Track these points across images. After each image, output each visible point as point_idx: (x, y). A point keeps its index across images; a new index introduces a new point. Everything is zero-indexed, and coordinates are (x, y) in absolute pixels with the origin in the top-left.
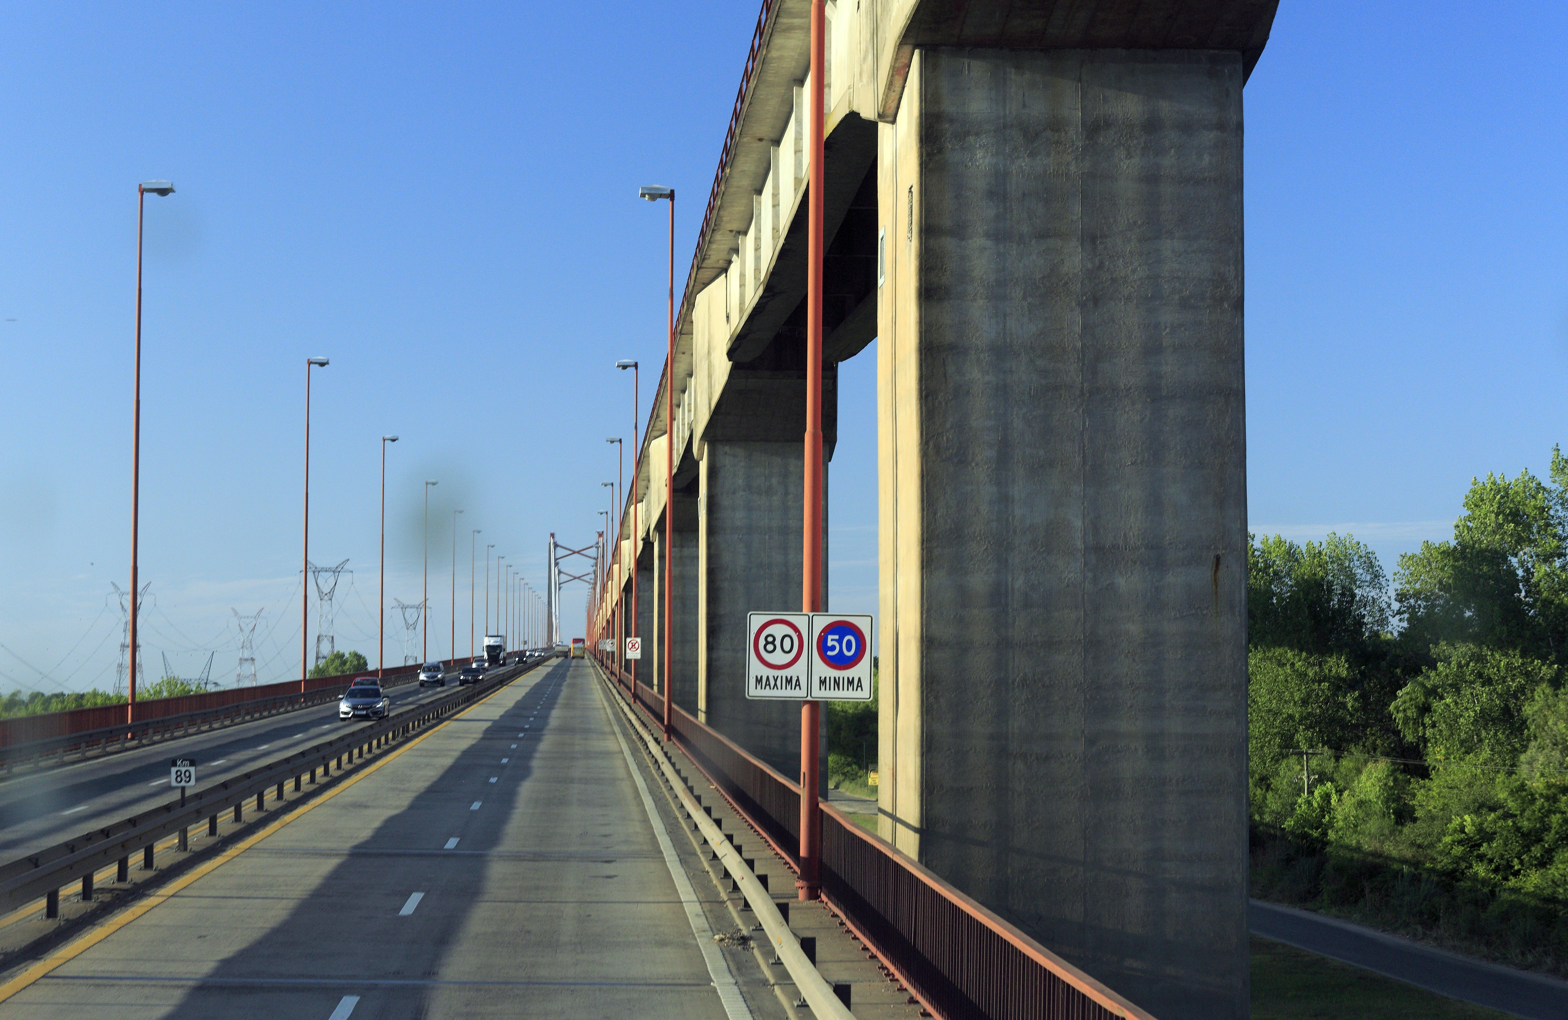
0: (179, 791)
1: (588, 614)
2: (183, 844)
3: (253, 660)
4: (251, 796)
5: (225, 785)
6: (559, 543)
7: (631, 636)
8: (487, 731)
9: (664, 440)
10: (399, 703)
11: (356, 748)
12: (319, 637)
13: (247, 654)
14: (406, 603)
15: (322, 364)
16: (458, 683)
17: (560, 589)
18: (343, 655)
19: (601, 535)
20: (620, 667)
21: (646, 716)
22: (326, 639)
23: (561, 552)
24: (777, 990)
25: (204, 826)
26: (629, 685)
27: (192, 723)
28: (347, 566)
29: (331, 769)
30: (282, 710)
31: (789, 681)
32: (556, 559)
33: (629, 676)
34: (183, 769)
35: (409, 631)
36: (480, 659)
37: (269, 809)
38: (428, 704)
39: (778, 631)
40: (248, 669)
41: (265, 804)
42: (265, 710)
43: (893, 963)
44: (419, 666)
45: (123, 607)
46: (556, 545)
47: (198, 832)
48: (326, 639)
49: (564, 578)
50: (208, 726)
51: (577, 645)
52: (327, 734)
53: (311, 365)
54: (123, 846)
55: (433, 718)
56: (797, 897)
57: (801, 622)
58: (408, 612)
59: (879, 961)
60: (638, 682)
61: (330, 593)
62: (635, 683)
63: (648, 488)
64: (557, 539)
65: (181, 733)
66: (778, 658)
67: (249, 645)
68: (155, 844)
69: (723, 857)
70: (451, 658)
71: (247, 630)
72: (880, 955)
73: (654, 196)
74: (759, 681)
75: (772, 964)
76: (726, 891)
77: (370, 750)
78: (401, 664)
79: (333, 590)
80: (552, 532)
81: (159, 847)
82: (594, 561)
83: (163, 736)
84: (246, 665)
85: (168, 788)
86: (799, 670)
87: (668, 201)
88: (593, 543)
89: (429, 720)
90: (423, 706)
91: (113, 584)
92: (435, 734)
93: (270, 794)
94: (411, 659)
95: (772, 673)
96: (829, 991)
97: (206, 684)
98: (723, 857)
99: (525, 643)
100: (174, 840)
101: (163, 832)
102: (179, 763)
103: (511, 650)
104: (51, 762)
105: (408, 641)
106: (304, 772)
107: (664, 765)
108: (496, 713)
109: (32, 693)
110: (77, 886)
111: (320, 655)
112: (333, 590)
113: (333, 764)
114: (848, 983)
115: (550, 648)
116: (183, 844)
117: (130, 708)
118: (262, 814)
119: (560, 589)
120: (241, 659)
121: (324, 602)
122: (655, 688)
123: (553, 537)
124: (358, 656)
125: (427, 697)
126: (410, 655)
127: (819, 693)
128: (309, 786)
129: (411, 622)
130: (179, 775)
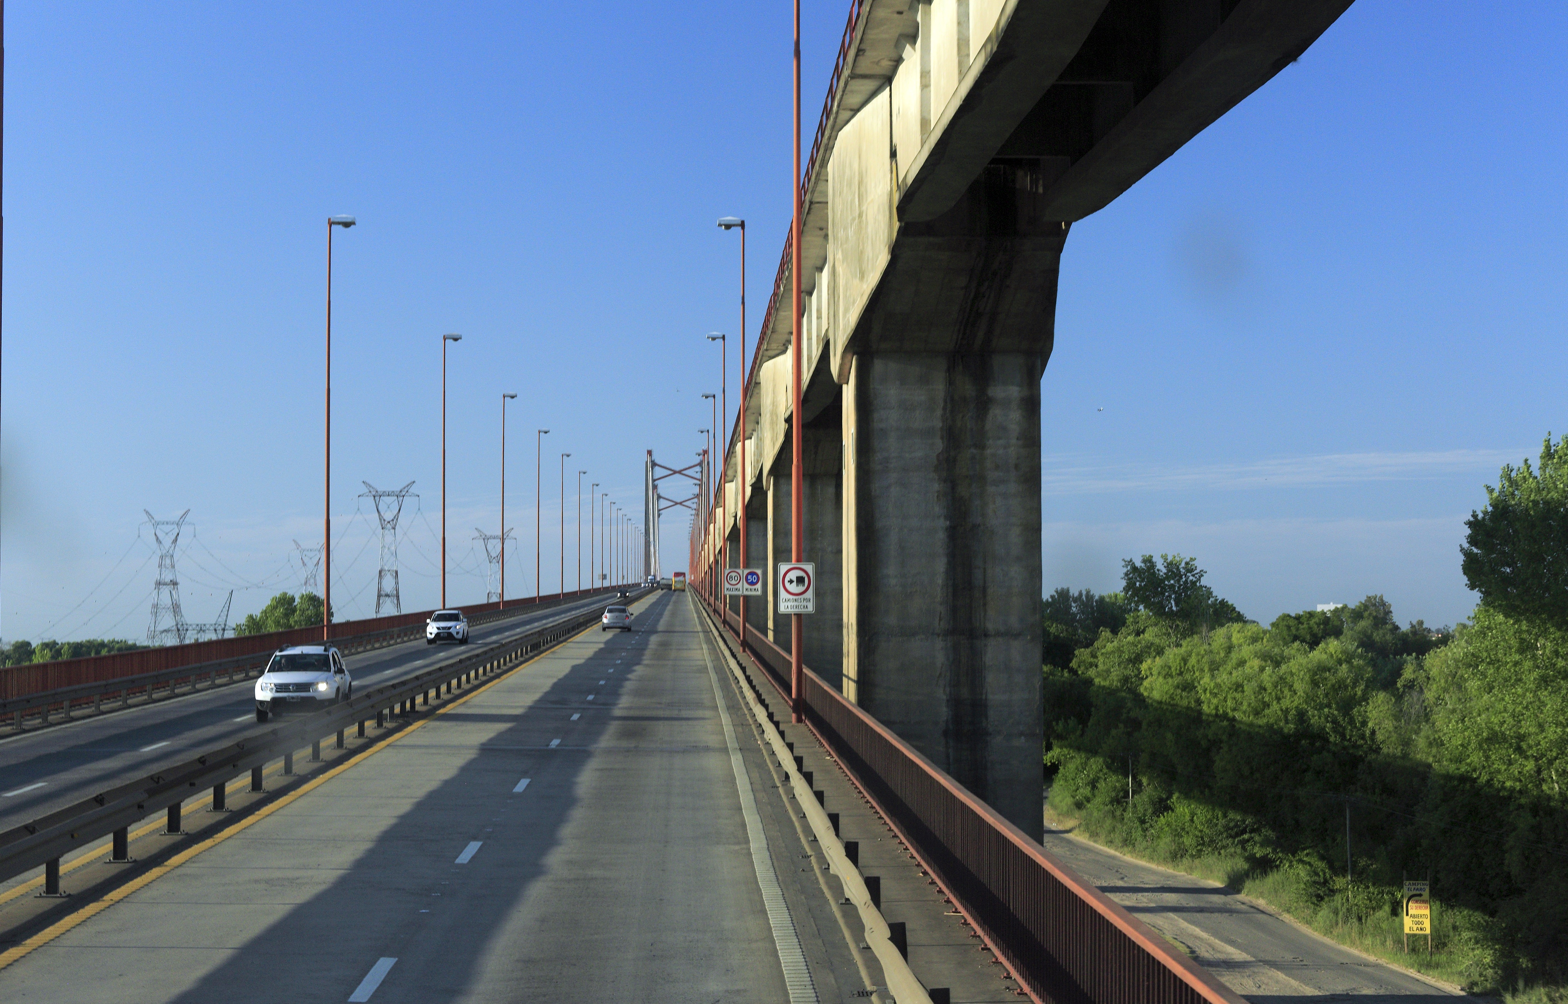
1: (691, 541)
2: (316, 754)
5: (99, 800)
6: (657, 461)
7: (789, 560)
8: (487, 749)
9: (786, 361)
10: (480, 642)
11: (463, 674)
12: (380, 572)
13: (168, 577)
14: (381, 489)
18: (293, 599)
21: (761, 678)
22: (389, 574)
23: (659, 472)
27: (201, 677)
30: (412, 637)
31: (736, 589)
32: (654, 481)
33: (737, 618)
35: (492, 564)
38: (550, 627)
39: (733, 574)
44: (429, 614)
45: (157, 539)
46: (654, 464)
48: (389, 574)
49: (663, 503)
50: (244, 675)
51: (678, 579)
57: (740, 571)
60: (747, 625)
61: (393, 520)
63: (758, 423)
66: (733, 582)
67: (312, 581)
71: (167, 541)
72: (923, 863)
74: (727, 589)
75: (863, 948)
76: (837, 902)
77: (459, 685)
78: (484, 601)
79: (396, 518)
81: (230, 787)
84: (165, 591)
86: (740, 586)
89: (511, 660)
90: (503, 645)
91: (147, 512)
94: (494, 596)
95: (731, 587)
97: (224, 630)
99: (604, 577)
105: (491, 575)
106: (453, 678)
109: (17, 642)
111: (382, 593)
112: (396, 518)
113: (432, 693)
114: (856, 841)
116: (340, 743)
121: (386, 531)
122: (771, 634)
125: (444, 657)
126: (493, 591)
127: (746, 593)
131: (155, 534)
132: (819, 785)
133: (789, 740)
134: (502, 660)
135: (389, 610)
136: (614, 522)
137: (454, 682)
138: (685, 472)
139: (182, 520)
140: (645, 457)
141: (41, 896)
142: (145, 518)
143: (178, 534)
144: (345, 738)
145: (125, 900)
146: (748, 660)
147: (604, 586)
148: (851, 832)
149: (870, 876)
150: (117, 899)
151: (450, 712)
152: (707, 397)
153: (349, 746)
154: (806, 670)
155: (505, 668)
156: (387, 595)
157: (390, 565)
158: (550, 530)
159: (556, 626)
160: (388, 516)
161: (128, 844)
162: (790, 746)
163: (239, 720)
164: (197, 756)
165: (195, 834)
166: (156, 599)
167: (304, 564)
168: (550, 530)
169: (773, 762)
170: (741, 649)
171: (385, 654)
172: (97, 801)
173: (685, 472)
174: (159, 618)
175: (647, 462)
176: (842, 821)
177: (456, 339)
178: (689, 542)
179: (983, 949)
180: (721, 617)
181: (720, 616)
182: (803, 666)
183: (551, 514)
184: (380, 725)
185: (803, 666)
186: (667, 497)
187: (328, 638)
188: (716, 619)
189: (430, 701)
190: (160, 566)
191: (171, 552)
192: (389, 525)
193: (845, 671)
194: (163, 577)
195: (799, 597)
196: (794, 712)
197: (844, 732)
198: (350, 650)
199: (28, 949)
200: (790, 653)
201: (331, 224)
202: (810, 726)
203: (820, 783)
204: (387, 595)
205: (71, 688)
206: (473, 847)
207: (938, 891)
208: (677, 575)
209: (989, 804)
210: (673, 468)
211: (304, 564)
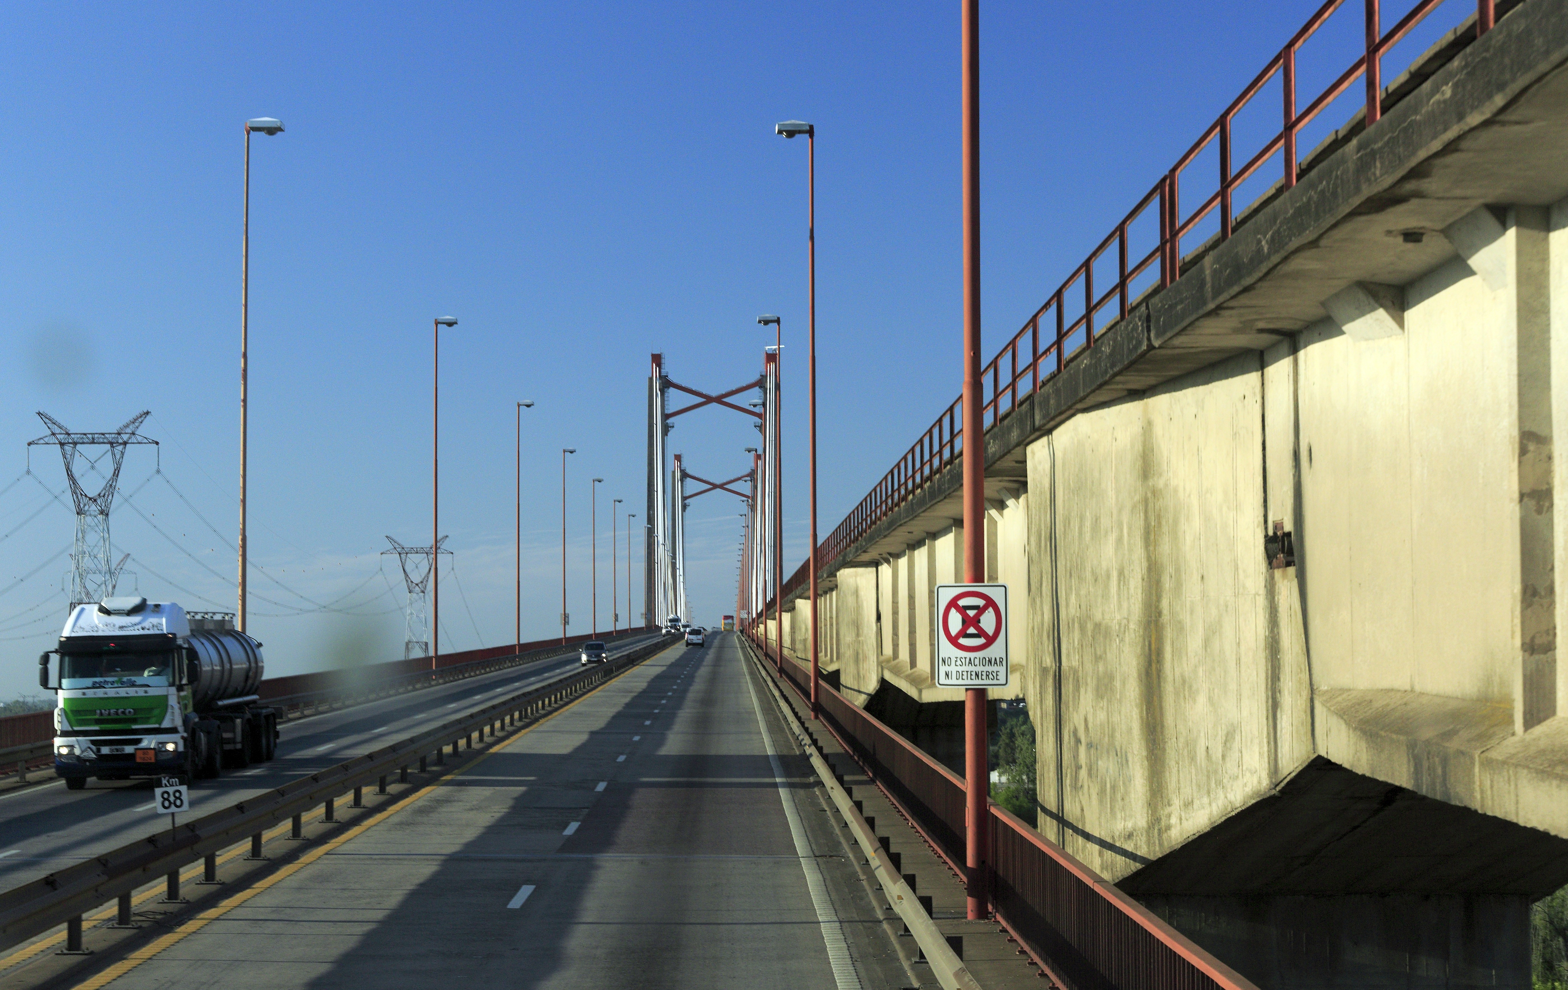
0: (170, 817)
4: (197, 859)
6: (673, 378)
11: (516, 711)
14: (407, 545)
17: (666, 429)
19: (771, 358)
23: (677, 400)
24: (885, 926)
28: (145, 429)
34: (171, 790)
37: (339, 819)
43: (1053, 970)
46: (666, 384)
51: (727, 621)
52: (569, 670)
53: (439, 325)
55: (520, 719)
56: (966, 918)
58: (413, 559)
59: (1039, 968)
64: (667, 368)
69: (877, 868)
70: (593, 632)
73: (767, 322)
77: (503, 727)
79: (111, 487)
80: (656, 352)
81: (305, 817)
82: (758, 421)
85: (155, 816)
87: (776, 324)
88: (754, 377)
96: (943, 941)
98: (877, 868)
100: (320, 810)
102: (164, 782)
103: (626, 627)
106: (486, 725)
107: (835, 791)
110: (111, 909)
112: (111, 487)
117: (434, 659)
119: (684, 507)
123: (659, 365)
129: (416, 578)
130: (165, 798)
137: (487, 729)
138: (728, 486)
145: (200, 931)
147: (569, 634)
151: (502, 751)
153: (94, 947)
155: (561, 703)
159: (519, 697)
160: (92, 486)
161: (181, 886)
162: (870, 822)
163: (376, 731)
164: (469, 714)
170: (778, 674)
173: (728, 486)
184: (382, 790)
186: (697, 476)
187: (436, 667)
188: (769, 664)
195: (972, 655)
196: (970, 895)
199: (181, 936)
200: (963, 775)
201: (564, 451)
202: (881, 787)
210: (704, 391)
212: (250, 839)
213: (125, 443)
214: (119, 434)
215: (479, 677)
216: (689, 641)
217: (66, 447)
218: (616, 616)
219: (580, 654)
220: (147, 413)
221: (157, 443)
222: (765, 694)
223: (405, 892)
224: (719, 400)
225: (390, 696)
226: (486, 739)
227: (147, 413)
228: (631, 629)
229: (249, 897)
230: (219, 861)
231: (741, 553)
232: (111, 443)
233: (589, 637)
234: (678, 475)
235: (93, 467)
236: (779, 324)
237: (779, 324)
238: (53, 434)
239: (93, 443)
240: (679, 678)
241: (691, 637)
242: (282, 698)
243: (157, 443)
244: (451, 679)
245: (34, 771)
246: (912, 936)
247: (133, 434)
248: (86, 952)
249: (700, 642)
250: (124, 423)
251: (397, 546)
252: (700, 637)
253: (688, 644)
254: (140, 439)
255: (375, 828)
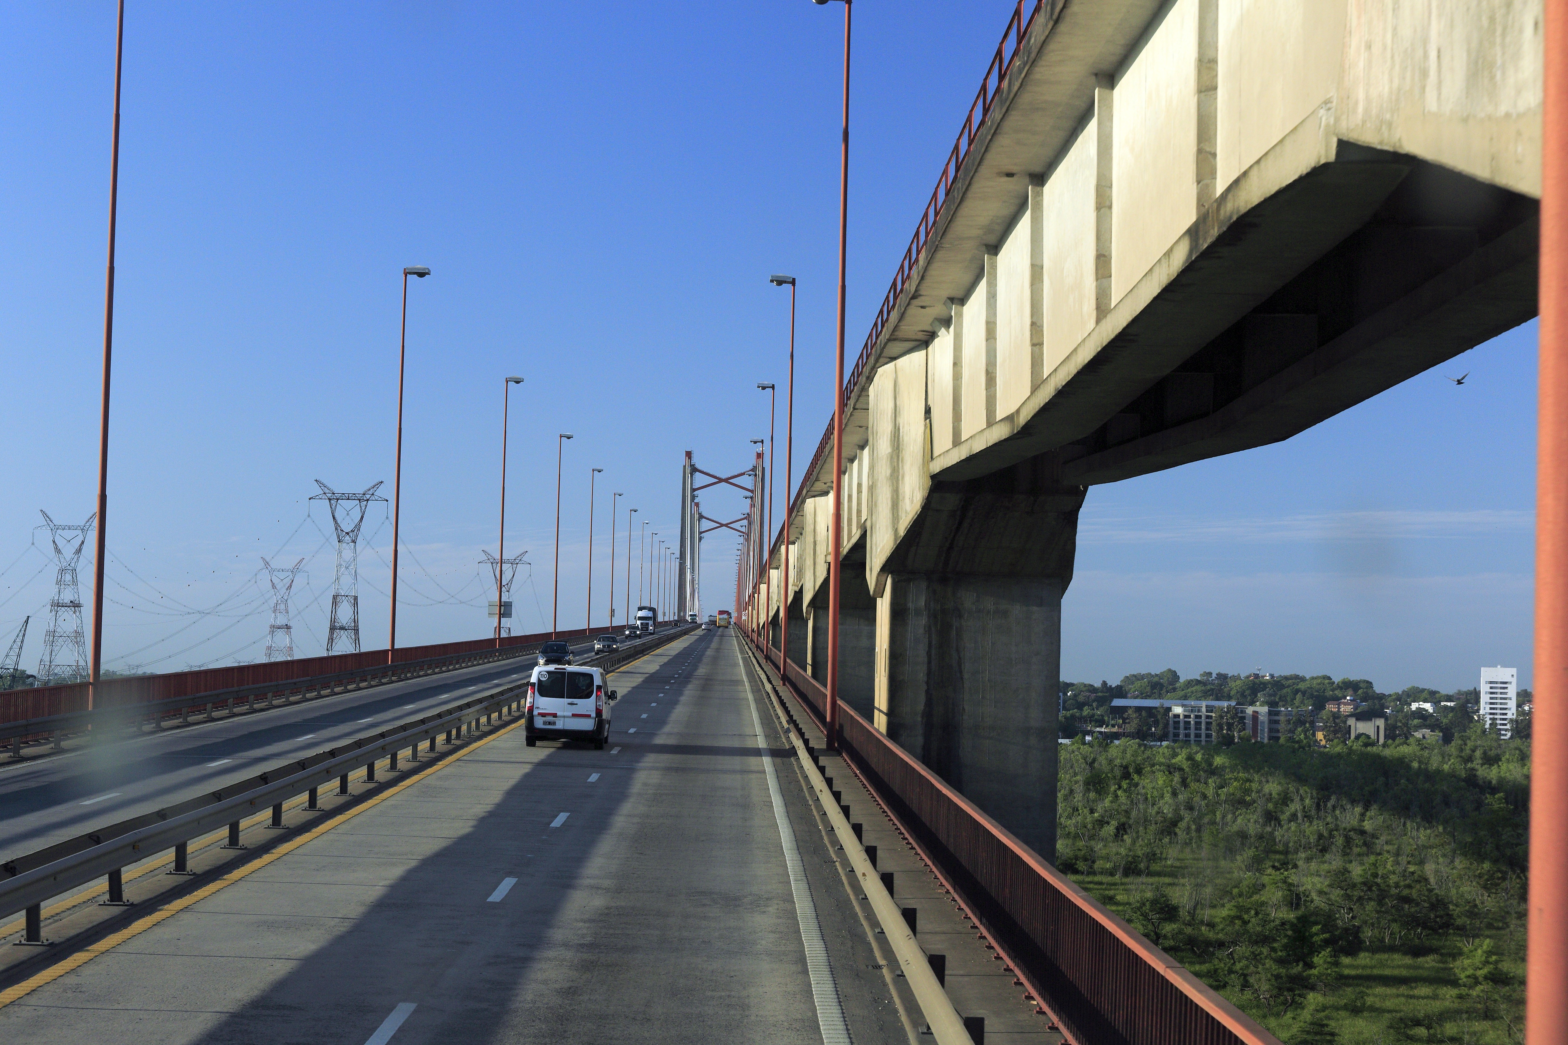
2: (393, 765)
3: (288, 627)
8: (647, 678)
13: (281, 620)
14: (339, 488)
15: (421, 275)
16: (594, 653)
17: (700, 539)
20: (768, 642)
22: (345, 602)
23: (700, 480)
25: (361, 772)
26: (821, 709)
27: (278, 694)
28: (380, 492)
29: (513, 710)
32: (693, 490)
33: (822, 689)
36: (633, 628)
40: (282, 639)
41: (419, 754)
42: (437, 667)
46: (694, 470)
47: (328, 791)
49: (706, 525)
51: (721, 616)
54: (327, 772)
60: (788, 660)
62: (834, 703)
65: (263, 705)
67: (282, 607)
68: (189, 842)
71: (68, 552)
77: (448, 740)
79: (358, 527)
81: (321, 789)
82: (749, 494)
83: (467, 664)
84: (280, 634)
92: (72, 980)
93: (382, 765)
101: (293, 790)
104: (175, 722)
108: (653, 668)
112: (358, 527)
115: (681, 620)
116: (393, 765)
118: (371, 786)
119: (700, 539)
120: (272, 627)
122: (809, 669)
124: (1170, 670)
128: (389, 773)
131: (54, 542)
132: (856, 818)
133: (855, 819)
134: (454, 732)
135: (344, 646)
136: (662, 558)
139: (88, 524)
140: (682, 460)
141: (225, 848)
142: (42, 520)
143: (83, 542)
144: (318, 794)
146: (786, 692)
148: (870, 838)
149: (971, 1016)
150: (104, 949)
152: (764, 388)
154: (840, 702)
156: (342, 628)
157: (346, 586)
158: (601, 567)
160: (347, 526)
165: (359, 796)
166: (52, 625)
167: (58, 551)
168: (601, 567)
169: (802, 776)
171: (490, 668)
172: (262, 779)
174: (56, 649)
175: (685, 467)
176: (897, 882)
177: (518, 382)
178: (736, 567)
179: (1038, 1012)
180: (763, 652)
181: (763, 652)
182: (837, 698)
183: (602, 549)
185: (837, 698)
188: (768, 668)
189: (492, 722)
190: (59, 582)
191: (73, 565)
192: (347, 538)
193: (876, 704)
194: (62, 596)
197: (874, 762)
198: (467, 664)
200: (825, 686)
203: (857, 816)
204: (342, 628)
205: (266, 684)
206: (497, 896)
207: (1015, 983)
208: (721, 612)
209: (967, 797)
211: (58, 551)
212: (339, 778)
213: (368, 500)
214: (364, 494)
215: (364, 692)
216: (539, 723)
217: (332, 502)
218: (613, 611)
219: (537, 658)
220: (382, 482)
221: (387, 501)
222: (756, 681)
223: (387, 883)
224: (726, 480)
225: (392, 682)
226: (482, 728)
227: (382, 482)
228: (613, 627)
229: (247, 874)
230: (419, 748)
231: (740, 547)
232: (360, 500)
233: (548, 635)
234: (697, 516)
235: (348, 514)
236: (773, 389)
237: (773, 389)
238: (325, 493)
239: (348, 499)
240: (668, 683)
241: (546, 704)
242: (377, 667)
243: (387, 501)
244: (409, 675)
245: (72, 738)
246: (932, 1034)
247: (373, 494)
248: (46, 943)
249: (588, 725)
250: (368, 488)
251: (327, 491)
252: (587, 705)
253: (534, 736)
254: (377, 498)
255: (332, 831)
